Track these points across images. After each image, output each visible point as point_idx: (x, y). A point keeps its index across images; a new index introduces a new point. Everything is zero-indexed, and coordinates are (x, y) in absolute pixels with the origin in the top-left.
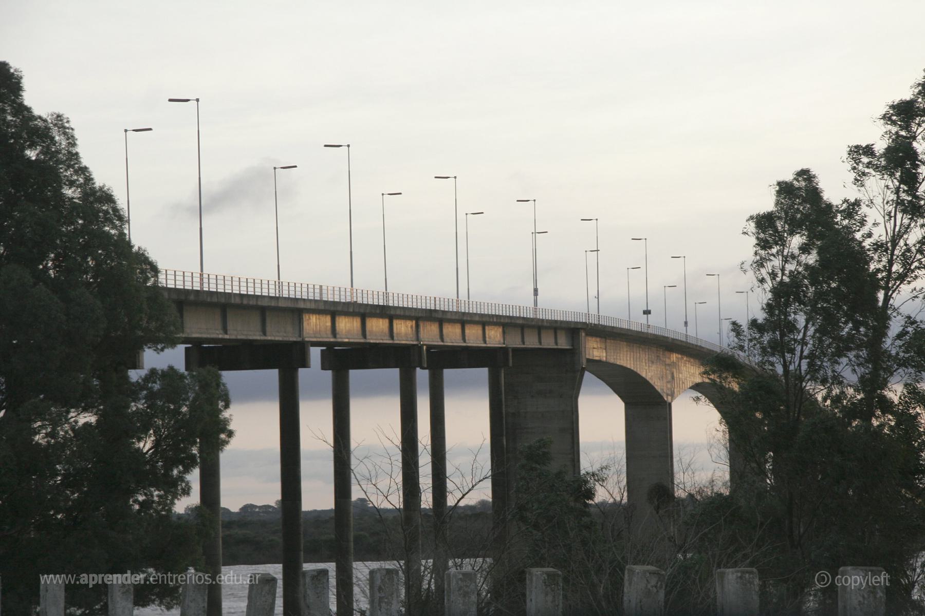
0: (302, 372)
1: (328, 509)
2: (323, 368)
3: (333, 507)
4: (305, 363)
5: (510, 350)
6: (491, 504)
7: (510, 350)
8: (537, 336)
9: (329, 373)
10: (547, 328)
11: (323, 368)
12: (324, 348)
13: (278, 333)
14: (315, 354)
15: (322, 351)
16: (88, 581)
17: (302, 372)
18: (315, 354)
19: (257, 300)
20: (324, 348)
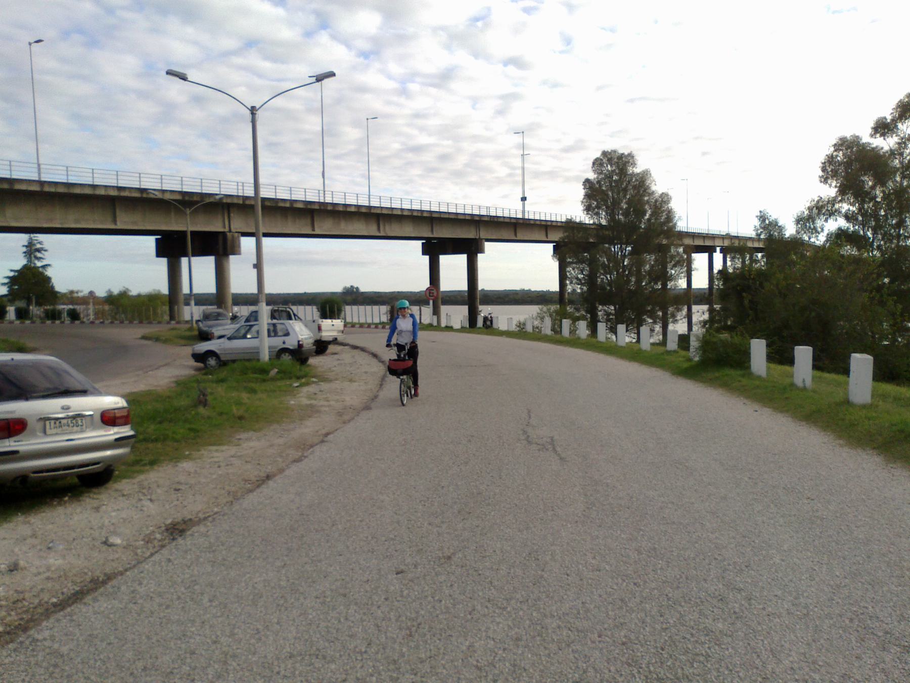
0: (714, 254)
1: (554, 290)
2: (423, 254)
3: (558, 290)
4: (715, 252)
5: (189, 234)
6: (467, 298)
7: (189, 234)
8: (545, 233)
9: (427, 258)
10: (718, 238)
11: (423, 254)
12: (424, 241)
13: (708, 243)
14: (718, 249)
15: (423, 243)
16: (220, 337)
17: (714, 254)
18: (718, 249)
19: (392, 211)
20: (424, 241)
